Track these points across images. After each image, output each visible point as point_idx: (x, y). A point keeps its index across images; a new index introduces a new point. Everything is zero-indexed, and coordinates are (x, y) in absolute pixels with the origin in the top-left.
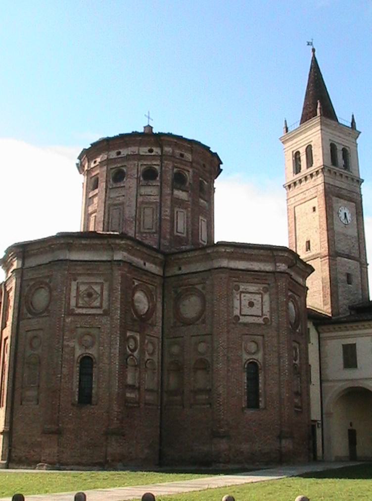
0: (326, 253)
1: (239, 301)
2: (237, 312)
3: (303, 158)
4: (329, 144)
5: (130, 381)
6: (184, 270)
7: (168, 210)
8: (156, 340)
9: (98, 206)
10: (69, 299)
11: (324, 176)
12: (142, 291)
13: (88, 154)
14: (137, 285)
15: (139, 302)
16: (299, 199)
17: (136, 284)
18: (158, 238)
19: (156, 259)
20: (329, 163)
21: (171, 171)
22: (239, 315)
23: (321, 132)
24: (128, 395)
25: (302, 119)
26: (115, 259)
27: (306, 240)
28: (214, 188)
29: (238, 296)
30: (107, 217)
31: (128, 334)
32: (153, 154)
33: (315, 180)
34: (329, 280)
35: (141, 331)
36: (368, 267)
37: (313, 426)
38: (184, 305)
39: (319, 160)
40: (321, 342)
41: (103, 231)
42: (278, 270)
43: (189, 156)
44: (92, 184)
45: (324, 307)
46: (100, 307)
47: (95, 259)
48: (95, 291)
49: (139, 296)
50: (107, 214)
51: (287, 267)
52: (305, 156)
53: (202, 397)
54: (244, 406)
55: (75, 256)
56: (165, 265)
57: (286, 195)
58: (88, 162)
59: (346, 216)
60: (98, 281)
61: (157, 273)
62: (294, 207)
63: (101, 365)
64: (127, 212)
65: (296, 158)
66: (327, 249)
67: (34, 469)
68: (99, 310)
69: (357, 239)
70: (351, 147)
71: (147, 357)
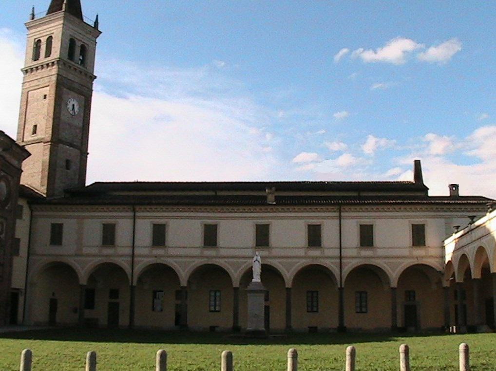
0: (49, 139)
3: (43, 47)
4: (69, 39)
11: (59, 68)
16: (34, 85)
36: (88, 156)
37: (15, 295)
39: (56, 54)
62: (28, 92)
65: (37, 45)
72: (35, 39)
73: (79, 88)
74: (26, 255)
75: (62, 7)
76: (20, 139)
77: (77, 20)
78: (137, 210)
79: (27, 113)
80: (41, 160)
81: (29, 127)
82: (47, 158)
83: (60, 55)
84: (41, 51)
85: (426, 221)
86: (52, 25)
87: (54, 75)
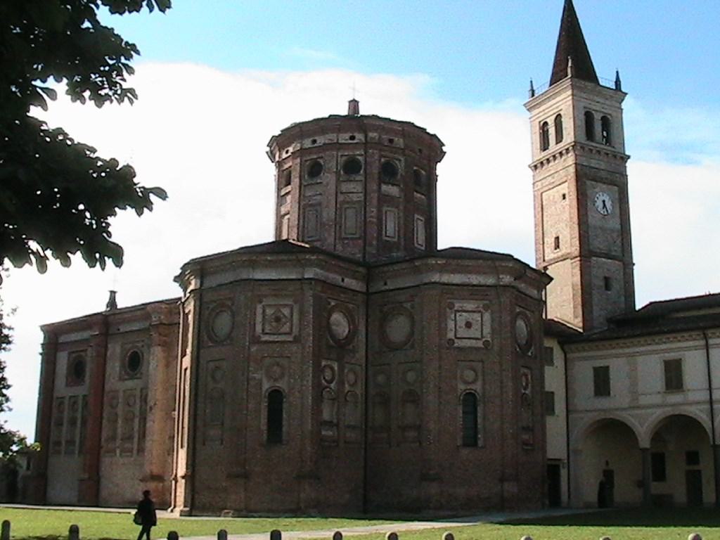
0: (577, 253)
1: (453, 322)
2: (451, 335)
3: (552, 131)
4: (583, 113)
5: (326, 415)
6: (390, 286)
7: (375, 210)
8: (358, 368)
9: (291, 207)
10: (255, 324)
11: (576, 155)
12: (341, 312)
13: (279, 142)
14: (334, 306)
15: (337, 326)
16: (547, 183)
17: (333, 304)
18: (362, 245)
19: (357, 274)
20: (583, 139)
21: (377, 162)
22: (453, 338)
23: (573, 98)
24: (323, 433)
25: (551, 81)
26: (306, 277)
27: (555, 236)
28: (437, 176)
30: (301, 221)
32: (355, 141)
33: (565, 160)
34: (580, 287)
35: (339, 360)
36: (635, 267)
37: (553, 469)
38: (390, 327)
39: (569, 136)
40: (568, 364)
41: (298, 241)
42: (501, 283)
43: (399, 142)
44: (284, 179)
45: (574, 320)
48: (284, 315)
49: (337, 317)
50: (301, 216)
51: (512, 279)
52: (554, 128)
53: (411, 434)
54: (459, 444)
55: (259, 275)
56: (368, 280)
57: (532, 178)
58: (280, 151)
59: (604, 205)
60: (286, 302)
61: (358, 289)
62: (542, 193)
63: (291, 399)
64: (325, 214)
65: (543, 131)
66: (578, 248)
67: (220, 516)
68: (287, 336)
69: (620, 233)
70: (614, 114)
71: (347, 387)
72: (540, 122)
73: (609, 176)
75: (567, 72)
76: (540, 258)
77: (590, 85)
78: (710, 335)
79: (545, 223)
80: (570, 283)
81: (550, 241)
82: (577, 279)
83: (575, 137)
84: (550, 137)
85: (684, 354)
86: (558, 99)
87: (571, 165)
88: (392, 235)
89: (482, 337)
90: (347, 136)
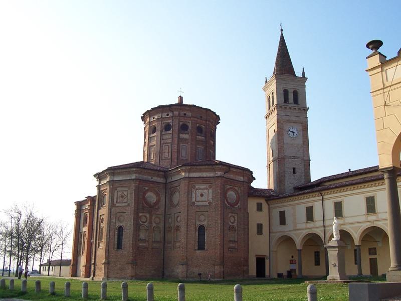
2: (194, 200)
29: (195, 191)
31: (140, 214)
35: (150, 213)
40: (270, 210)
43: (189, 114)
46: (117, 202)
47: (124, 179)
56: (166, 177)
71: (154, 225)
74: (268, 233)
88: (185, 156)
89: (208, 200)
90: (166, 114)
